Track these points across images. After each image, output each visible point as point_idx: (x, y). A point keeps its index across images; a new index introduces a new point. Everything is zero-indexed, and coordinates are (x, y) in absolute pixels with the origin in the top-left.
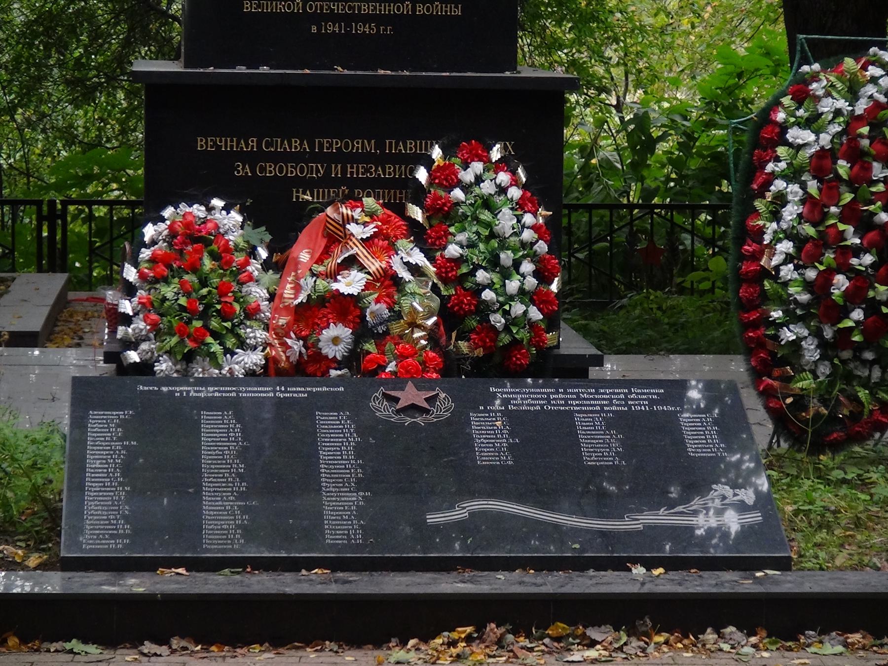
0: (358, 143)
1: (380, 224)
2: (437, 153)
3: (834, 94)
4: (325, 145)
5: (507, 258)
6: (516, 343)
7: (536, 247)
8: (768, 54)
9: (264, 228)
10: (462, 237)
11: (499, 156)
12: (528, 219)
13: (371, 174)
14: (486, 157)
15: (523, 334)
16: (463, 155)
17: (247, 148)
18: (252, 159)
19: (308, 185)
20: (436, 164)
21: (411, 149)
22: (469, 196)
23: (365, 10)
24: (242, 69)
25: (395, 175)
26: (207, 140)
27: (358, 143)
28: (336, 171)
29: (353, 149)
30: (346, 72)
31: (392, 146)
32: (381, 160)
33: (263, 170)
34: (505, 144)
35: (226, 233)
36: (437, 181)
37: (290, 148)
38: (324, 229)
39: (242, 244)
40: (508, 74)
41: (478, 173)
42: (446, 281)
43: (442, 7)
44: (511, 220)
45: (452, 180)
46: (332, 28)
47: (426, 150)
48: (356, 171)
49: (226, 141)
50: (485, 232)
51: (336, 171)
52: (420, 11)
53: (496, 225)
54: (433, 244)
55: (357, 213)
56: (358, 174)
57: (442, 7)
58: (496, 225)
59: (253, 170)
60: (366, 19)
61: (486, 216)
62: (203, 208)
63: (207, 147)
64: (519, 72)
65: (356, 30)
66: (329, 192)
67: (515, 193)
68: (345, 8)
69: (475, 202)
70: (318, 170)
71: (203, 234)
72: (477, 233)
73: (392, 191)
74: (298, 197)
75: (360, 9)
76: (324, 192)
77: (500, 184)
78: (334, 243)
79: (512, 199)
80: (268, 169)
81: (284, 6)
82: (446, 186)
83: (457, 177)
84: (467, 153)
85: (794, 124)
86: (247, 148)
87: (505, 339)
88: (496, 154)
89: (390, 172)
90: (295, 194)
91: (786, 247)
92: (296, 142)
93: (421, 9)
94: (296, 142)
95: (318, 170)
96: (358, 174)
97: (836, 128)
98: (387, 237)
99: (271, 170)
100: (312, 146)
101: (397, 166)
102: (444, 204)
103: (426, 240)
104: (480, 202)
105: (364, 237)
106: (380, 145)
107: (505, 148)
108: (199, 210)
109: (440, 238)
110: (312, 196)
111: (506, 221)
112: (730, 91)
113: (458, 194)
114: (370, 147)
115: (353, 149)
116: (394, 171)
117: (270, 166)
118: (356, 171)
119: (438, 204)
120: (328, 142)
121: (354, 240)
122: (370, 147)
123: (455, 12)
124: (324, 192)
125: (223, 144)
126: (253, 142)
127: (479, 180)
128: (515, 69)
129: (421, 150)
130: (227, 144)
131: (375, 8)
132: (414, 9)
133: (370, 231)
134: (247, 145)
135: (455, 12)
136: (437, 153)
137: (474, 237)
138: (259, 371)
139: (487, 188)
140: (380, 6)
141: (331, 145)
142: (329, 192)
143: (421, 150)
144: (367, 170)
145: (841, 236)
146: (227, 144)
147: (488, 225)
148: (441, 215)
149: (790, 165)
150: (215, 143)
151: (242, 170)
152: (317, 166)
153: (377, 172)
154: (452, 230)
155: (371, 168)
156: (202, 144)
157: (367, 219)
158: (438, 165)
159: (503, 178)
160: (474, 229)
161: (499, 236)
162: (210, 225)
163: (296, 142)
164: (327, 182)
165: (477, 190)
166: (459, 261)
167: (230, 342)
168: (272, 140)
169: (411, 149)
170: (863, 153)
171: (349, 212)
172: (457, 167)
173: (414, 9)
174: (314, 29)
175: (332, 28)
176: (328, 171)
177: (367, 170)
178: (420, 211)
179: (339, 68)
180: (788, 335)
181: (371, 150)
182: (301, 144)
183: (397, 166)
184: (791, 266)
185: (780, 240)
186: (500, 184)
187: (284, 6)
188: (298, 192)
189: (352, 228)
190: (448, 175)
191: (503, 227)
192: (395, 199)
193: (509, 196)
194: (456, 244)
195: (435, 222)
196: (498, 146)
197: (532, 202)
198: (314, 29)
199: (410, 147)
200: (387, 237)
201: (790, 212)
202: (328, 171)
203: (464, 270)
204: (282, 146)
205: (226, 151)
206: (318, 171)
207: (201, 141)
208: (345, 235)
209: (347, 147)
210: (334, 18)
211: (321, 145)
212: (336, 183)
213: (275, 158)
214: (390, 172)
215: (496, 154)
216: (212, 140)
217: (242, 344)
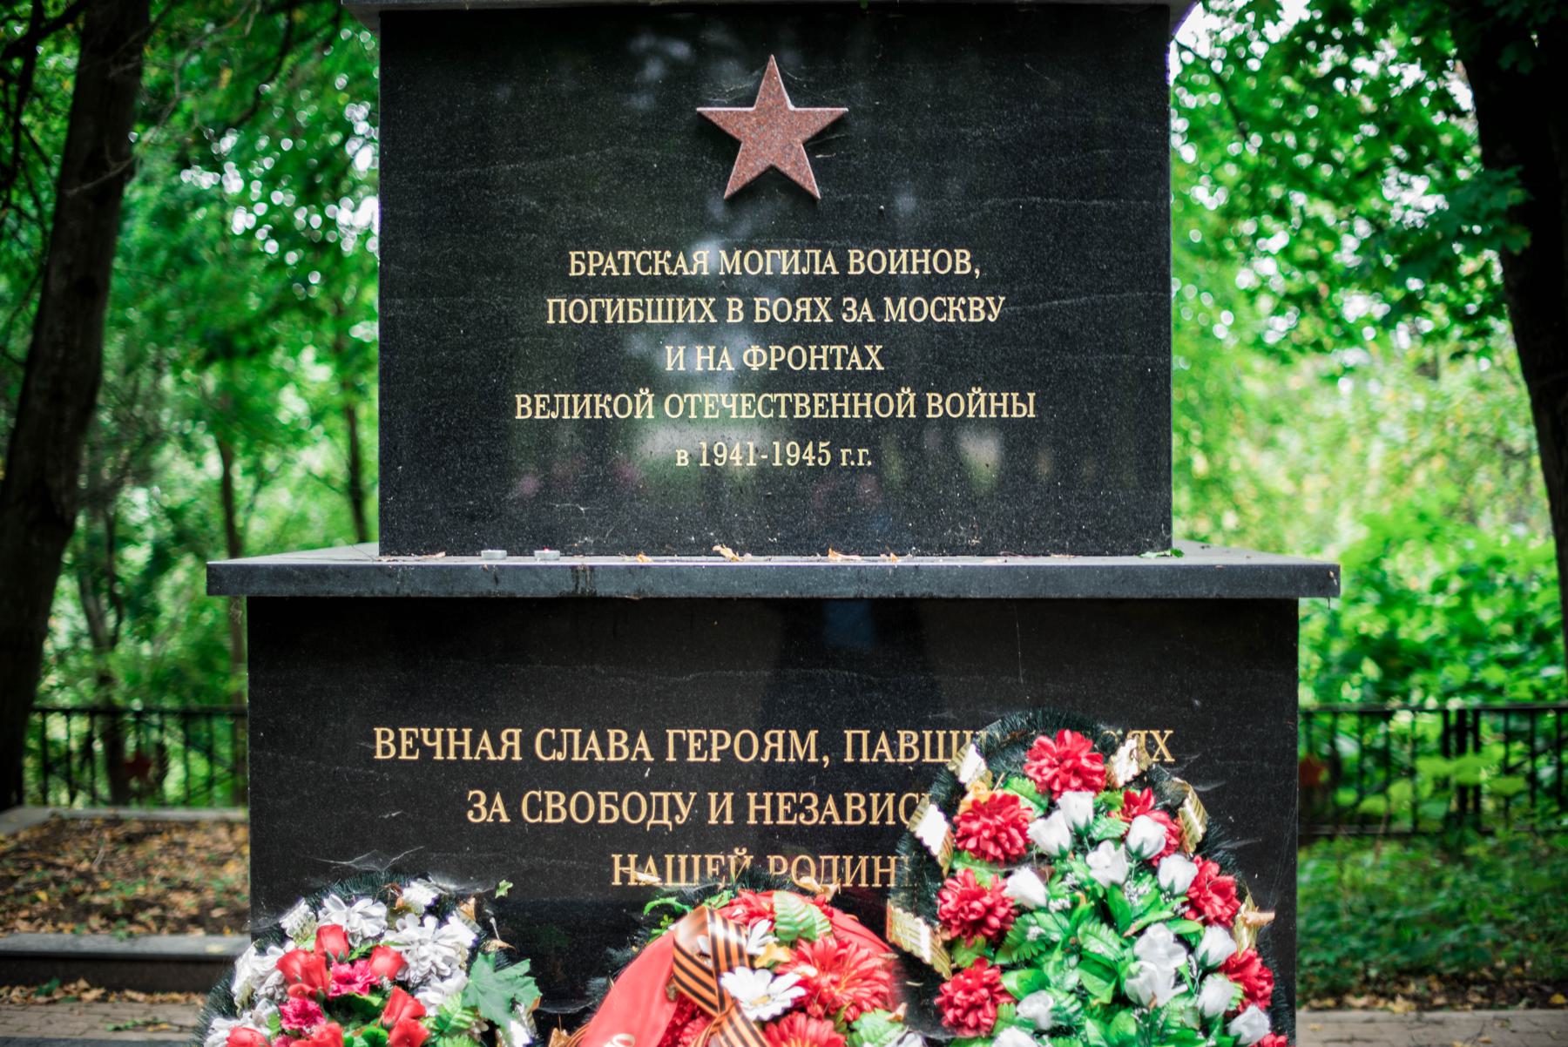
0: (774, 738)
1: (811, 971)
2: (970, 766)
4: (692, 744)
7: (1237, 1025)
8: (1422, 517)
9: (525, 966)
11: (1134, 770)
12: (1216, 944)
13: (809, 816)
14: (1101, 774)
16: (1039, 771)
17: (497, 752)
18: (508, 780)
19: (650, 844)
20: (969, 798)
21: (909, 752)
22: (1056, 885)
23: (803, 411)
25: (869, 817)
26: (398, 735)
27: (774, 738)
28: (720, 809)
29: (761, 753)
30: (749, 560)
31: (865, 746)
32: (835, 779)
33: (537, 807)
34: (1149, 737)
35: (425, 981)
36: (972, 843)
37: (605, 752)
38: (668, 982)
39: (459, 1016)
40: (1150, 558)
41: (1081, 823)
43: (988, 400)
44: (1171, 954)
45: (1011, 840)
47: (948, 754)
49: (445, 736)
50: (1102, 993)
52: (935, 410)
53: (1131, 976)
54: (958, 1024)
55: (758, 940)
56: (775, 816)
57: (988, 400)
58: (1131, 976)
59: (514, 811)
61: (1101, 942)
62: (380, 910)
63: (398, 752)
64: (1178, 554)
65: (784, 457)
66: (703, 862)
67: (1179, 872)
68: (754, 406)
69: (1075, 904)
70: (670, 809)
71: (354, 990)
72: (1081, 993)
73: (863, 859)
74: (625, 877)
75: (790, 407)
76: (689, 863)
77: (1138, 852)
78: (693, 1017)
79: (1171, 889)
80: (550, 805)
81: (610, 404)
82: (995, 859)
83: (1023, 832)
84: (1051, 766)
86: (497, 752)
88: (1125, 765)
89: (858, 809)
90: (617, 868)
92: (618, 738)
94: (618, 738)
95: (670, 809)
96: (775, 816)
98: (831, 1010)
99: (558, 807)
100: (658, 747)
101: (875, 797)
102: (990, 910)
103: (940, 1014)
104: (1085, 905)
105: (766, 1016)
106: (831, 744)
107: (1151, 746)
108: (366, 916)
109: (975, 1007)
110: (662, 873)
111: (1155, 965)
112: (1375, 563)
113: (1025, 884)
114: (805, 747)
115: (761, 753)
116: (868, 807)
117: (556, 799)
119: (972, 911)
120: (698, 737)
121: (737, 1019)
122: (805, 747)
123: (1020, 410)
124: (689, 863)
125: (438, 743)
126: (512, 738)
127: (1083, 841)
128: (1167, 544)
129: (934, 754)
130: (449, 743)
131: (828, 405)
132: (921, 405)
133: (785, 992)
134: (497, 746)
135: (1020, 410)
136: (970, 766)
137: (1070, 1004)
139: (1106, 866)
140: (840, 400)
141: (707, 746)
142: (703, 862)
143: (934, 754)
144: (798, 808)
147: (1110, 971)
148: (980, 940)
150: (418, 742)
151: (486, 809)
152: (672, 799)
153: (821, 812)
154: (1010, 981)
155: (808, 801)
156: (390, 743)
157: (783, 954)
158: (975, 803)
159: (1148, 831)
160: (1072, 979)
161: (1139, 1005)
162: (381, 963)
163: (617, 739)
164: (698, 837)
165: (1078, 869)
168: (559, 735)
169: (909, 752)
171: (734, 939)
172: (1024, 803)
173: (921, 405)
176: (702, 806)
177: (798, 808)
178: (925, 930)
179: (728, 552)
181: (807, 755)
182: (631, 743)
183: (875, 797)
186: (1138, 852)
187: (610, 404)
188: (625, 862)
189: (738, 983)
190: (999, 829)
191: (1150, 981)
192: (870, 879)
193: (1164, 881)
194: (1022, 1024)
195: (965, 957)
196: (1131, 743)
197: (1221, 890)
199: (907, 746)
200: (831, 1010)
204: (580, 746)
205: (446, 762)
206: (674, 810)
207: (385, 736)
208: (722, 999)
209: (746, 750)
211: (682, 747)
212: (721, 839)
213: (570, 777)
214: (858, 809)
215: (1125, 765)
216: (409, 735)
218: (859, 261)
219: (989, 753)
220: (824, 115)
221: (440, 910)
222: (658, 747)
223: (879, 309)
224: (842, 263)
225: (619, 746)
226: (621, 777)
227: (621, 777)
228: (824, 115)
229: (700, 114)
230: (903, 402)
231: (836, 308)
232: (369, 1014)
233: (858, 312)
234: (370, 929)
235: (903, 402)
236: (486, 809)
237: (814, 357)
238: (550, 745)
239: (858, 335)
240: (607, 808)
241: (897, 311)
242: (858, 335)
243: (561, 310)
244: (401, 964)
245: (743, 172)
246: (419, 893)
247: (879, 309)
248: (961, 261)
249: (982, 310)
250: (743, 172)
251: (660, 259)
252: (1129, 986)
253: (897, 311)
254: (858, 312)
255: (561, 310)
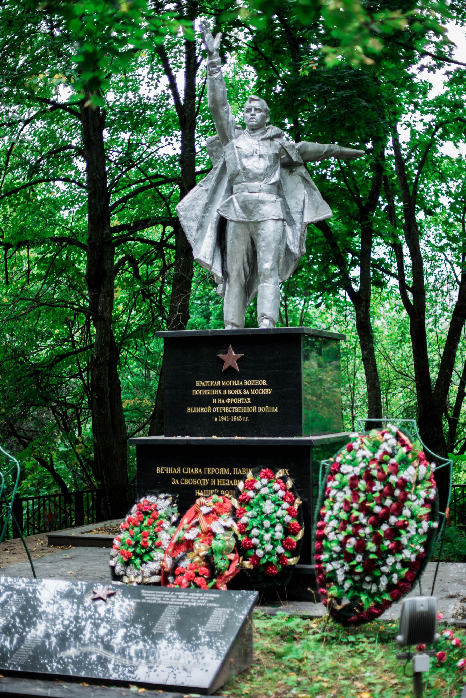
3: (365, 447)
5: (267, 523)
6: (269, 564)
10: (249, 513)
15: (274, 559)
18: (179, 477)
24: (179, 438)
28: (213, 482)
30: (220, 438)
33: (183, 481)
42: (242, 533)
46: (223, 419)
48: (221, 482)
51: (213, 482)
59: (179, 482)
60: (238, 414)
62: (155, 498)
70: (205, 482)
85: (344, 463)
87: (264, 561)
91: (334, 523)
93: (260, 409)
95: (205, 482)
97: (362, 465)
99: (187, 482)
100: (203, 471)
106: (231, 471)
114: (227, 471)
118: (221, 482)
122: (227, 471)
126: (179, 469)
130: (169, 470)
132: (257, 409)
136: (250, 475)
138: (157, 571)
144: (226, 482)
145: (357, 518)
146: (169, 470)
149: (340, 483)
151: (175, 482)
156: (159, 470)
162: (153, 506)
164: (209, 487)
166: (246, 525)
167: (146, 558)
170: (373, 478)
173: (257, 409)
174: (216, 419)
175: (223, 419)
176: (210, 482)
177: (226, 482)
180: (329, 567)
184: (333, 533)
185: (331, 520)
198: (216, 419)
201: (337, 506)
202: (210, 482)
203: (248, 529)
204: (191, 471)
210: (224, 414)
211: (207, 471)
217: (152, 560)
218: (246, 383)
219: (254, 473)
220: (240, 355)
221: (166, 498)
222: (203, 471)
223: (250, 392)
224: (243, 383)
225: (196, 471)
226: (197, 476)
227: (197, 476)
228: (240, 355)
229: (218, 357)
230: (254, 409)
231: (242, 391)
232: (150, 514)
233: (246, 392)
234: (153, 501)
235: (254, 409)
236: (175, 482)
237: (238, 401)
238: (185, 471)
239: (246, 396)
240: (195, 482)
241: (253, 392)
242: (246, 396)
243: (195, 392)
244: (156, 506)
245: (225, 367)
246: (162, 496)
247: (250, 392)
248: (264, 382)
249: (268, 391)
250: (225, 367)
251: (212, 383)
252: (263, 510)
253: (253, 392)
254: (246, 392)
255: (195, 392)
